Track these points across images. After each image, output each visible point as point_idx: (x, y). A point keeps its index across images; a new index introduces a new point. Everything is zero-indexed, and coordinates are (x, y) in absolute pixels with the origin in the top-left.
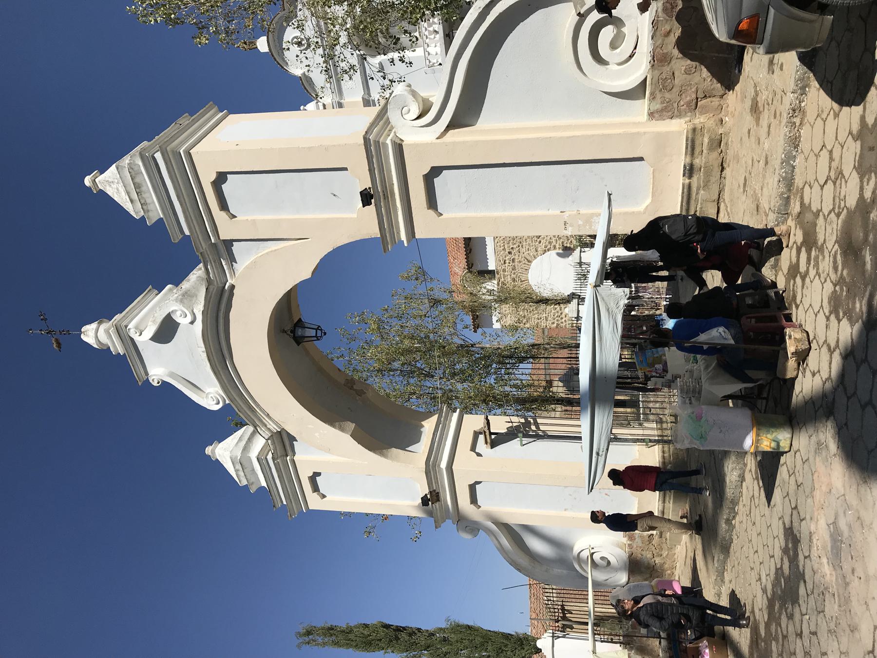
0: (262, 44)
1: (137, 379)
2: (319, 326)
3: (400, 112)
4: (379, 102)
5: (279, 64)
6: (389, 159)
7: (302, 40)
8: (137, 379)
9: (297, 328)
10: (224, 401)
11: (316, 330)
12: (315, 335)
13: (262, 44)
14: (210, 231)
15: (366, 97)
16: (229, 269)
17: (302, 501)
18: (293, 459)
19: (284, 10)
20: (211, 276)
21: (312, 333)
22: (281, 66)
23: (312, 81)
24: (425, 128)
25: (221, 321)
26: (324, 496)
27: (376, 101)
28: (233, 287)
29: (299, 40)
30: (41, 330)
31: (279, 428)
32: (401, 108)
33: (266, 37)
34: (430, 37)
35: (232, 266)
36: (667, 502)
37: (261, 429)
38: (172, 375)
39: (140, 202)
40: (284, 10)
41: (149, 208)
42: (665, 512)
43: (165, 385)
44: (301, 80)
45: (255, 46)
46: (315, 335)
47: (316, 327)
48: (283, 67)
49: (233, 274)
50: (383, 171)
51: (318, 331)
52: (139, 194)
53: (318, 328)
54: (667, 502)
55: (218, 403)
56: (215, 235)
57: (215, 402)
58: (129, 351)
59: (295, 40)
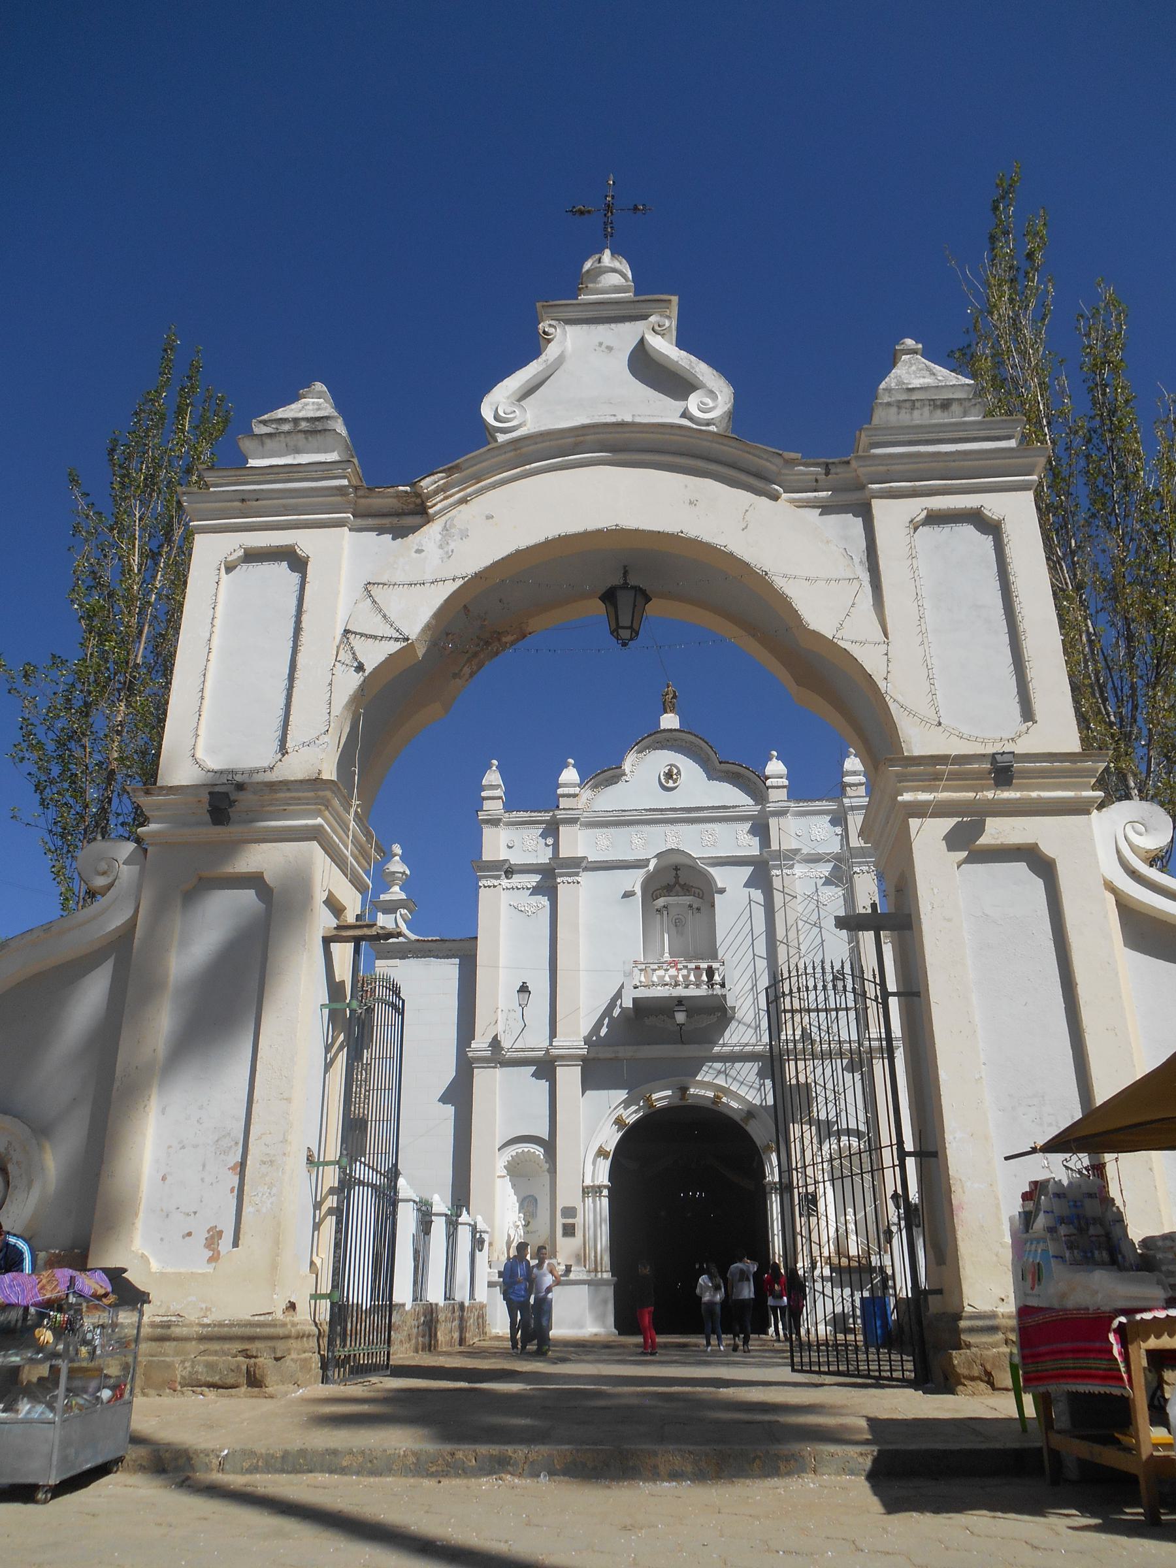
0: (670, 721)
1: (551, 303)
2: (637, 634)
3: (1136, 820)
4: (574, 883)
5: (642, 740)
6: (1048, 791)
7: (675, 781)
8: (551, 303)
9: (632, 593)
10: (504, 431)
11: (631, 628)
12: (621, 625)
13: (670, 721)
14: (891, 487)
15: (584, 865)
16: (808, 500)
17: (581, 458)
18: (345, 526)
19: (720, 763)
20: (802, 468)
21: (625, 621)
22: (639, 743)
23: (612, 784)
24: (1116, 856)
25: (701, 464)
26: (229, 569)
27: (577, 878)
28: (775, 497)
29: (675, 777)
30: (613, 197)
31: (436, 513)
32: (1144, 822)
33: (678, 727)
34: (667, 976)
35: (818, 507)
36: (202, 1347)
37: (442, 478)
38: (560, 360)
39: (917, 400)
40: (720, 763)
41: (904, 411)
42: (168, 1343)
43: (532, 347)
44: (617, 768)
45: (668, 710)
46: (621, 625)
47: (635, 626)
48: (637, 744)
49: (801, 504)
50: (1043, 778)
51: (629, 631)
52: (932, 403)
53: (635, 633)
54: (202, 1347)
55: (497, 418)
56: (882, 492)
57: (501, 413)
58: (580, 308)
59: (675, 771)
